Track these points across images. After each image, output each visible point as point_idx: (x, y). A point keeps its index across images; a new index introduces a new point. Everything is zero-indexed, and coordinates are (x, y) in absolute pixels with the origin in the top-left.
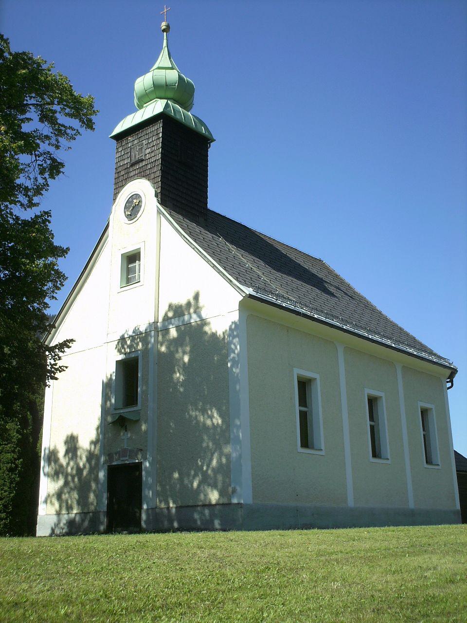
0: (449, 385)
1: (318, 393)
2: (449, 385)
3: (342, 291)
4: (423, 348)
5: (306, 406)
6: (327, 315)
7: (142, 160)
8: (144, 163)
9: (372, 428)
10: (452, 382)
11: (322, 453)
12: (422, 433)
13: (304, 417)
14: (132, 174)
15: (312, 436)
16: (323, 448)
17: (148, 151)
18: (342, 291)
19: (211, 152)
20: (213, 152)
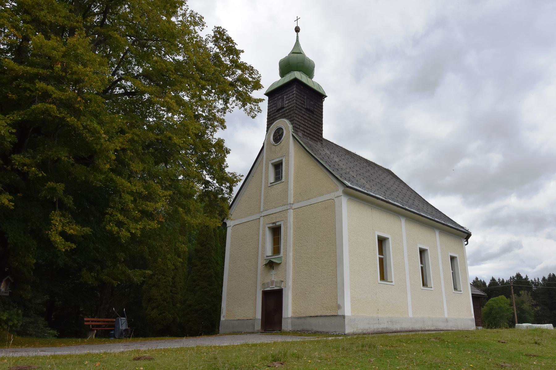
0: (466, 243)
1: (391, 246)
2: (466, 243)
3: (315, 333)
4: (454, 223)
5: (382, 255)
6: (418, 210)
7: (283, 108)
8: (285, 109)
9: (422, 268)
10: (467, 241)
11: (393, 283)
12: (451, 271)
13: (381, 261)
14: (277, 116)
15: (386, 267)
16: (393, 280)
17: (287, 102)
18: (315, 333)
19: (325, 103)
20: (326, 103)
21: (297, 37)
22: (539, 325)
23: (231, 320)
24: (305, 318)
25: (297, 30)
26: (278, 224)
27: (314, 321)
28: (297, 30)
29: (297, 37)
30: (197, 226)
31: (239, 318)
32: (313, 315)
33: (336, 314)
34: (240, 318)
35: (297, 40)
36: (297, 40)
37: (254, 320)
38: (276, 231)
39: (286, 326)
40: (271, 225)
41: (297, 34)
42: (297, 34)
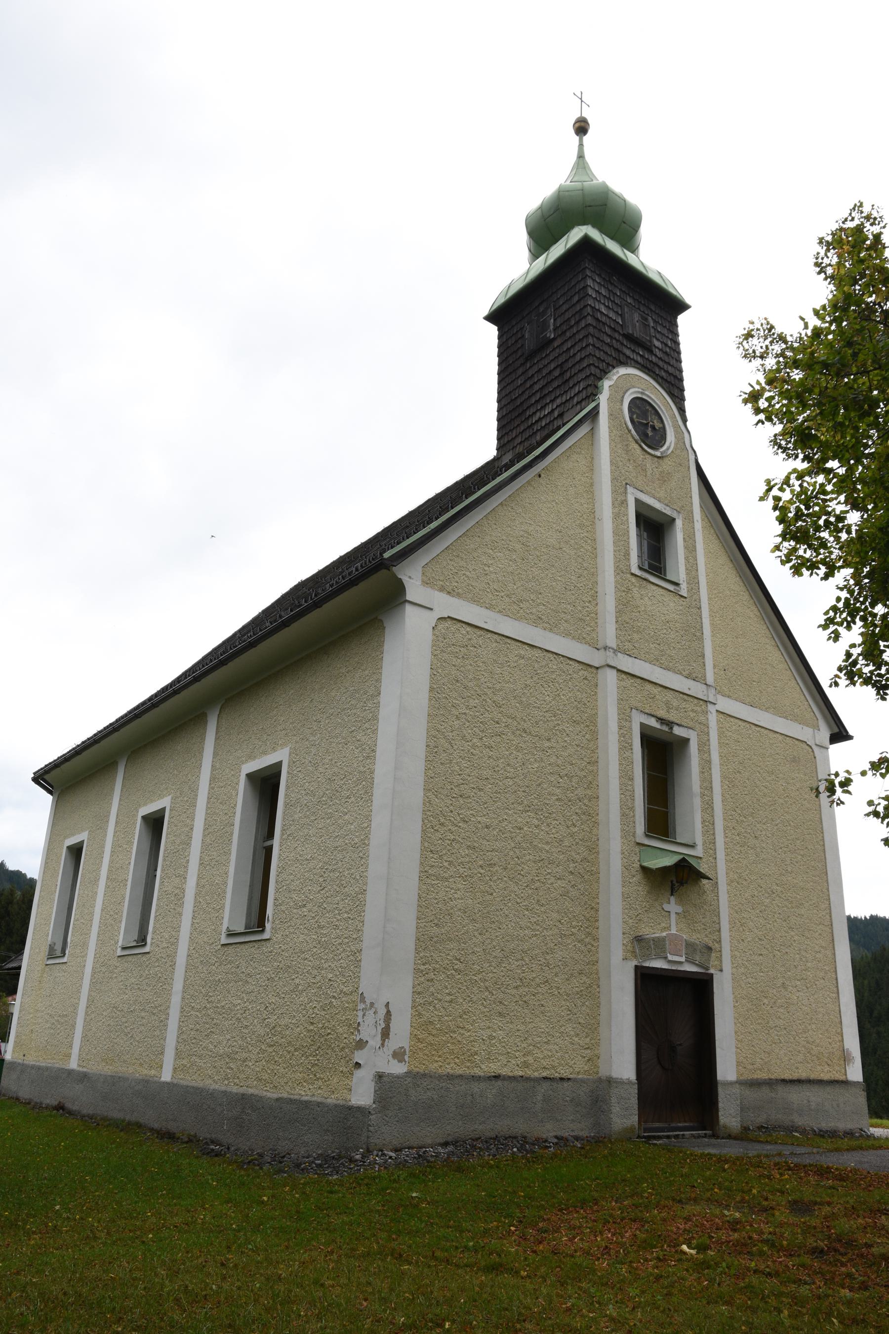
21: (581, 145)
22: (673, 968)
23: (450, 1077)
24: (771, 1083)
25: (581, 128)
26: (677, 731)
27: (795, 1096)
28: (581, 128)
29: (581, 145)
30: (797, 457)
31: (493, 1068)
32: (787, 1076)
33: (842, 1078)
34: (505, 1071)
35: (581, 156)
36: (581, 156)
37: (601, 1089)
38: (662, 754)
39: (729, 1115)
40: (653, 723)
41: (581, 141)
42: (581, 141)
